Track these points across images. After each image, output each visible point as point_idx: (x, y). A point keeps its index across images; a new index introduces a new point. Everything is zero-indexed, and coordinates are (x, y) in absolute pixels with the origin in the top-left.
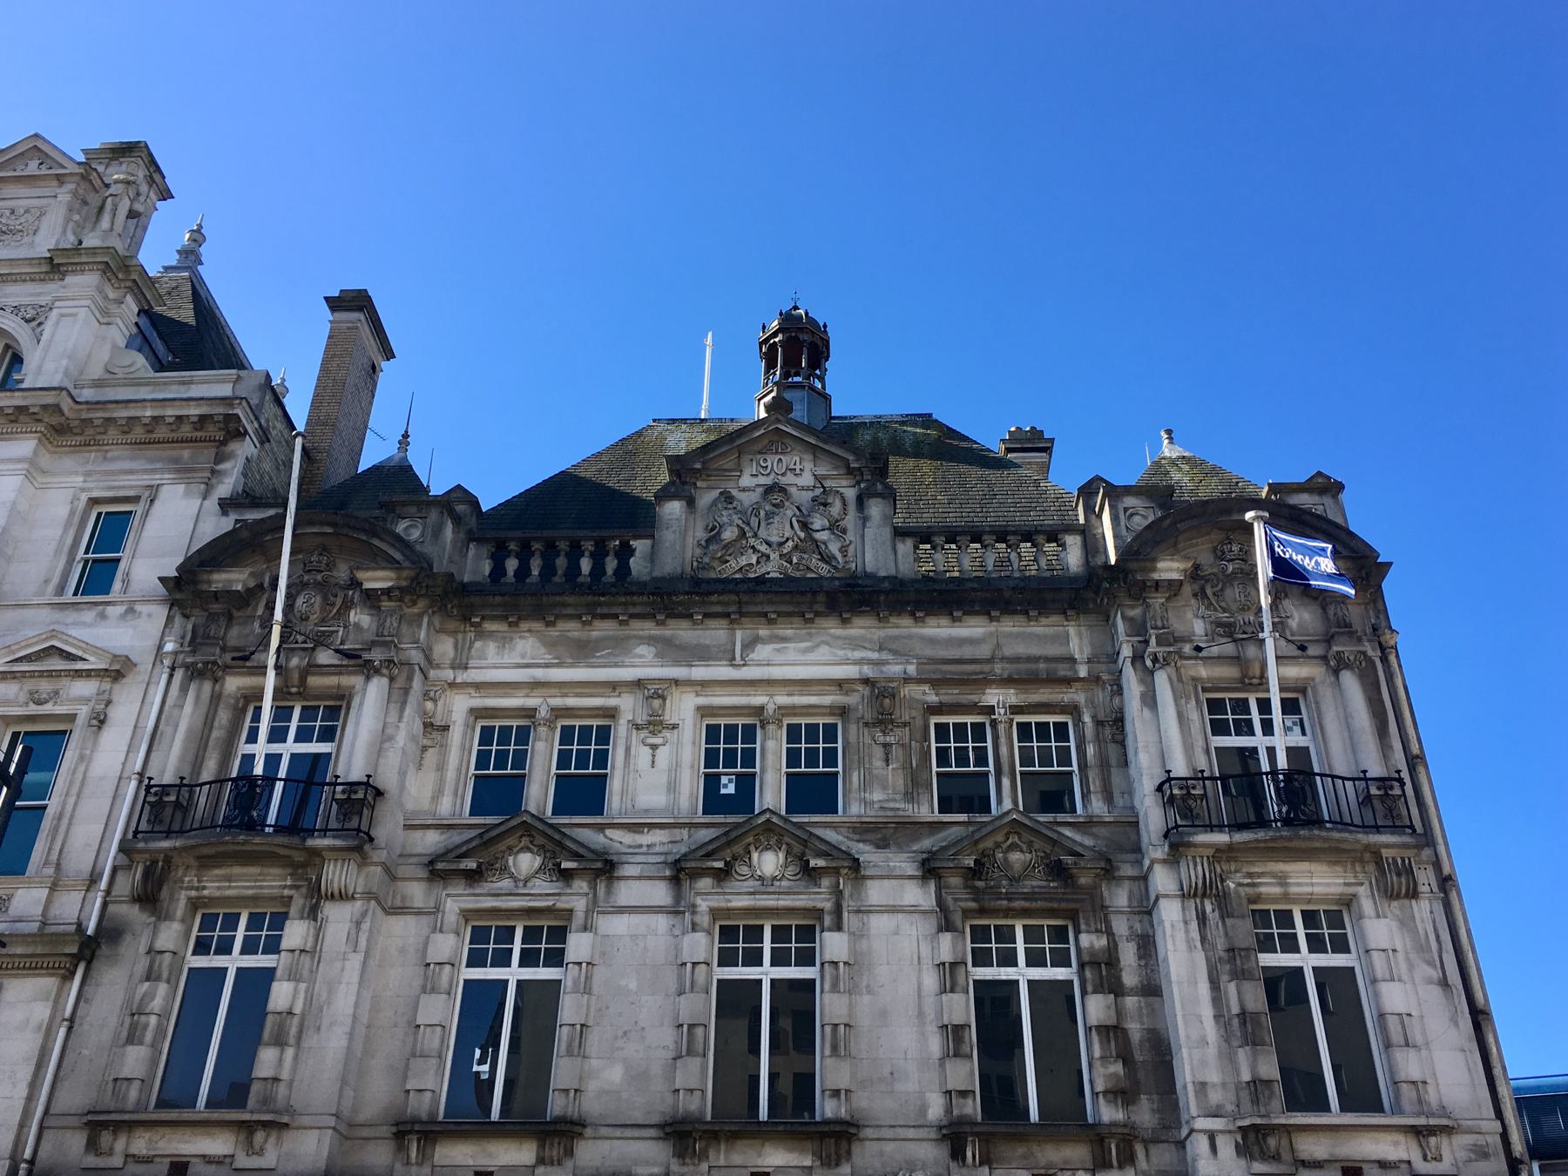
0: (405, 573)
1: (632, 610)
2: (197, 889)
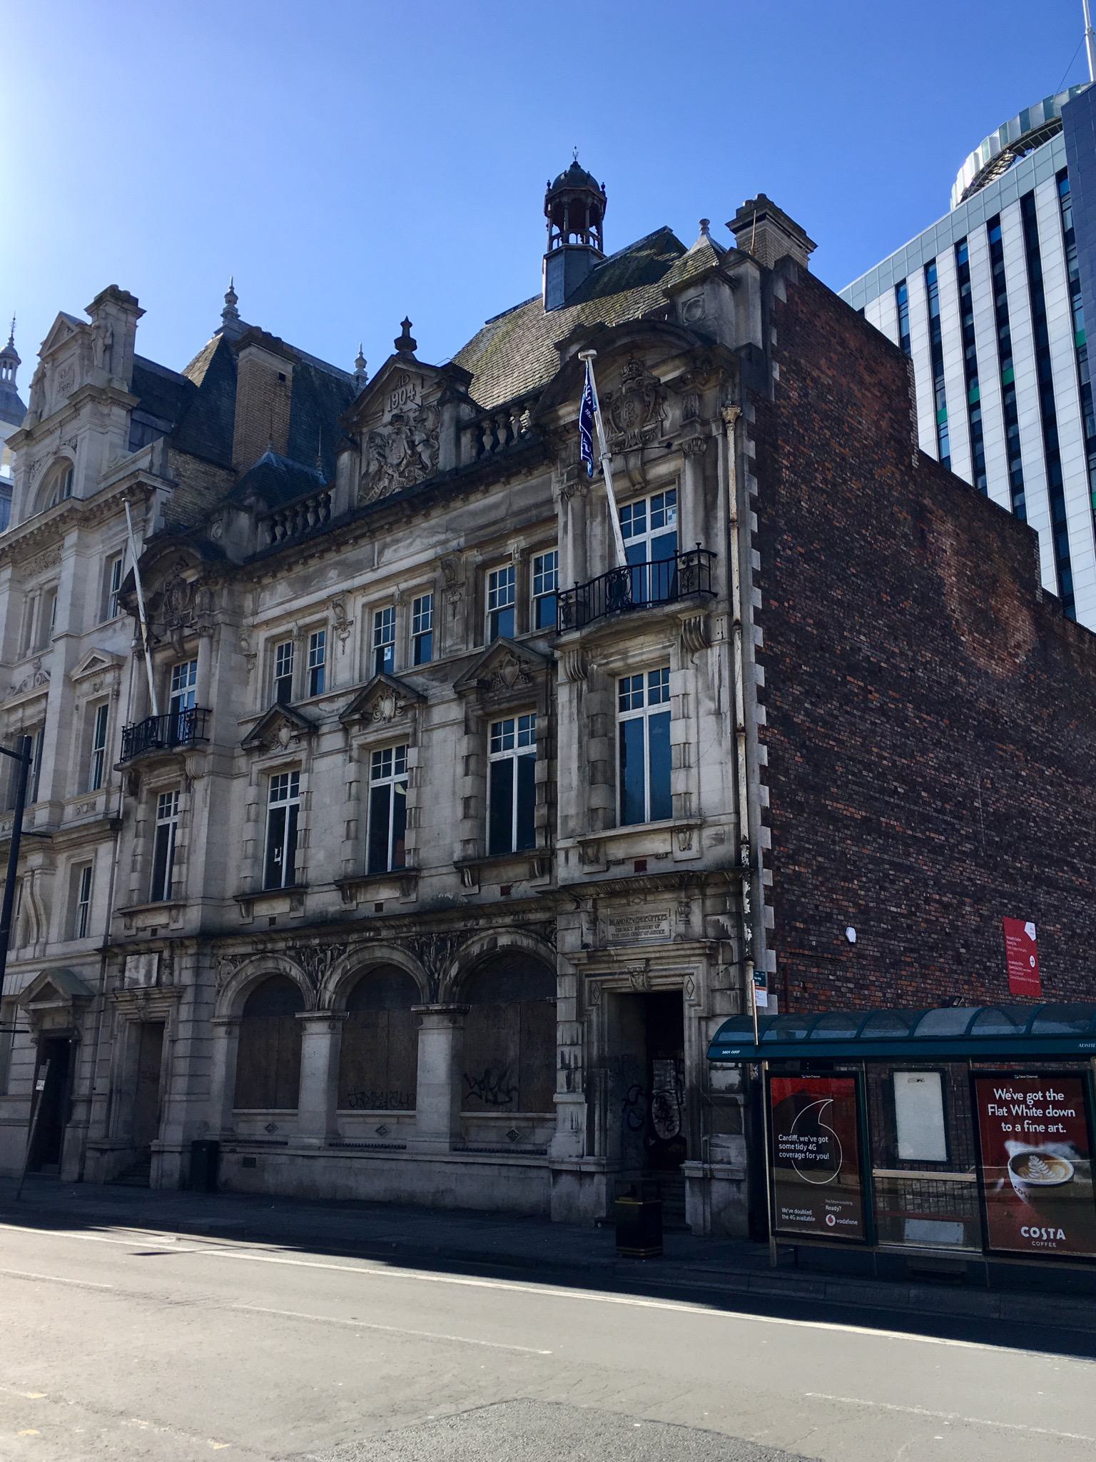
1: (321, 548)
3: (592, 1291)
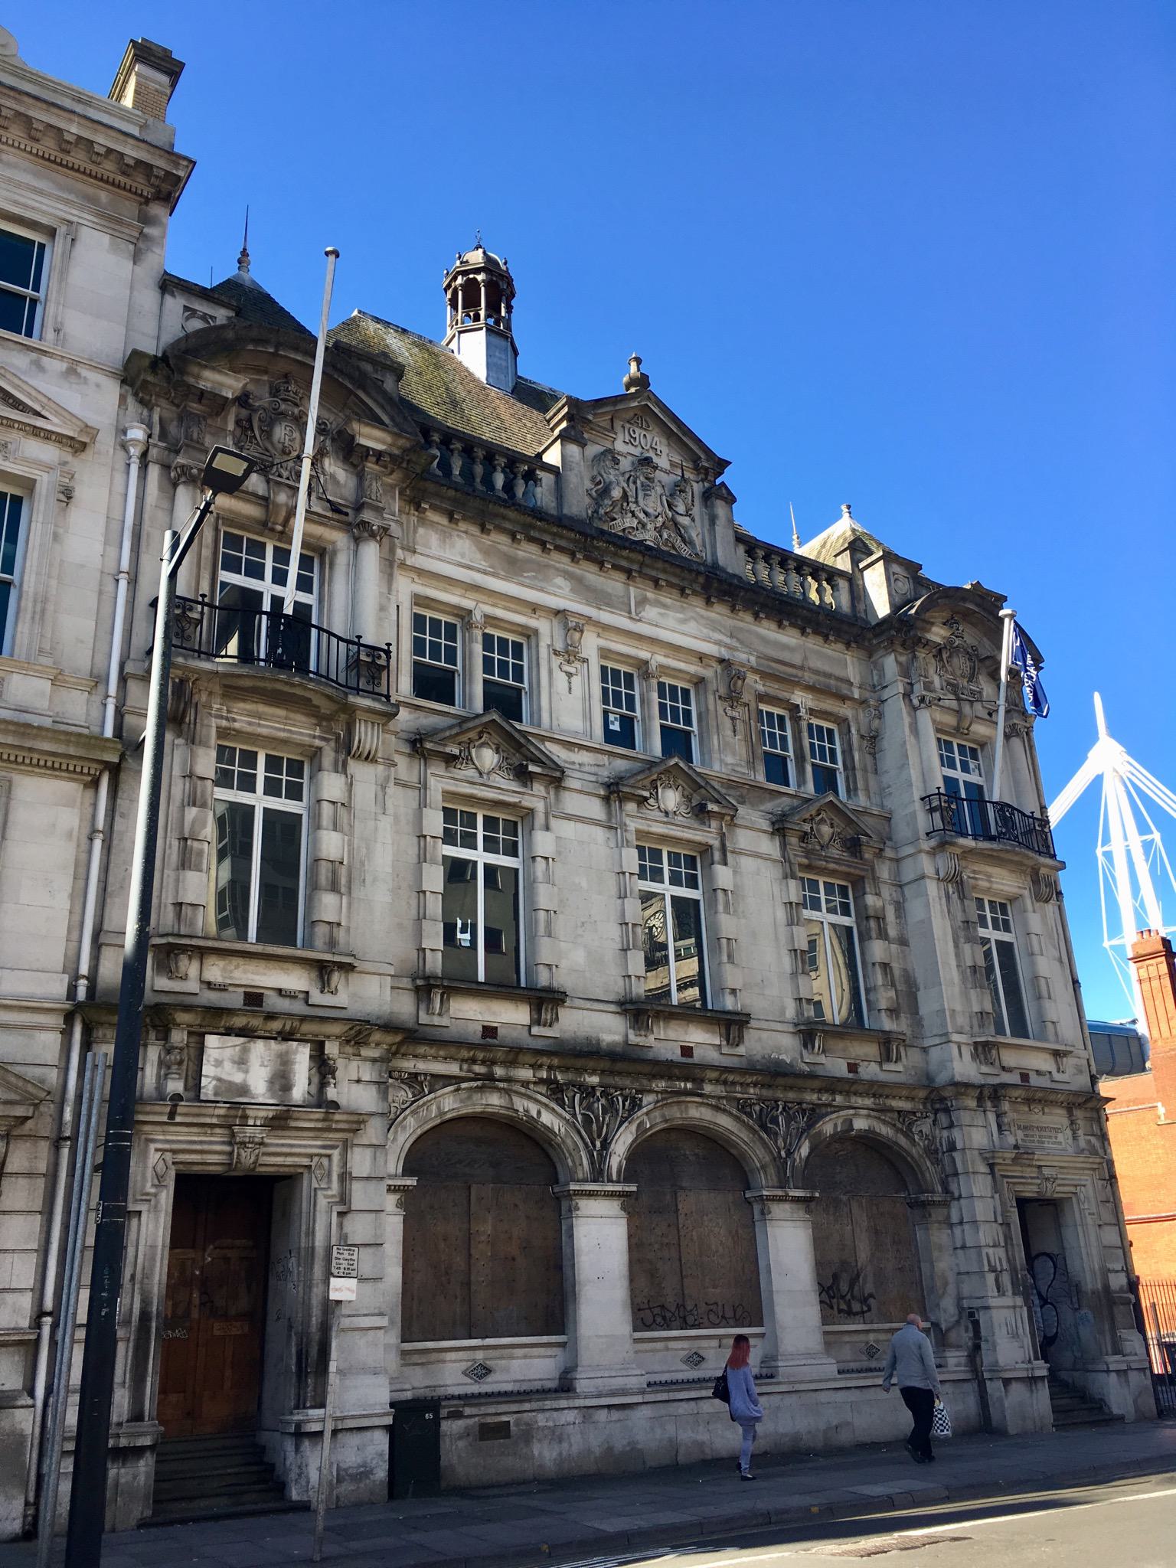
0: (401, 442)
2: (227, 719)
3: (841, 1540)
